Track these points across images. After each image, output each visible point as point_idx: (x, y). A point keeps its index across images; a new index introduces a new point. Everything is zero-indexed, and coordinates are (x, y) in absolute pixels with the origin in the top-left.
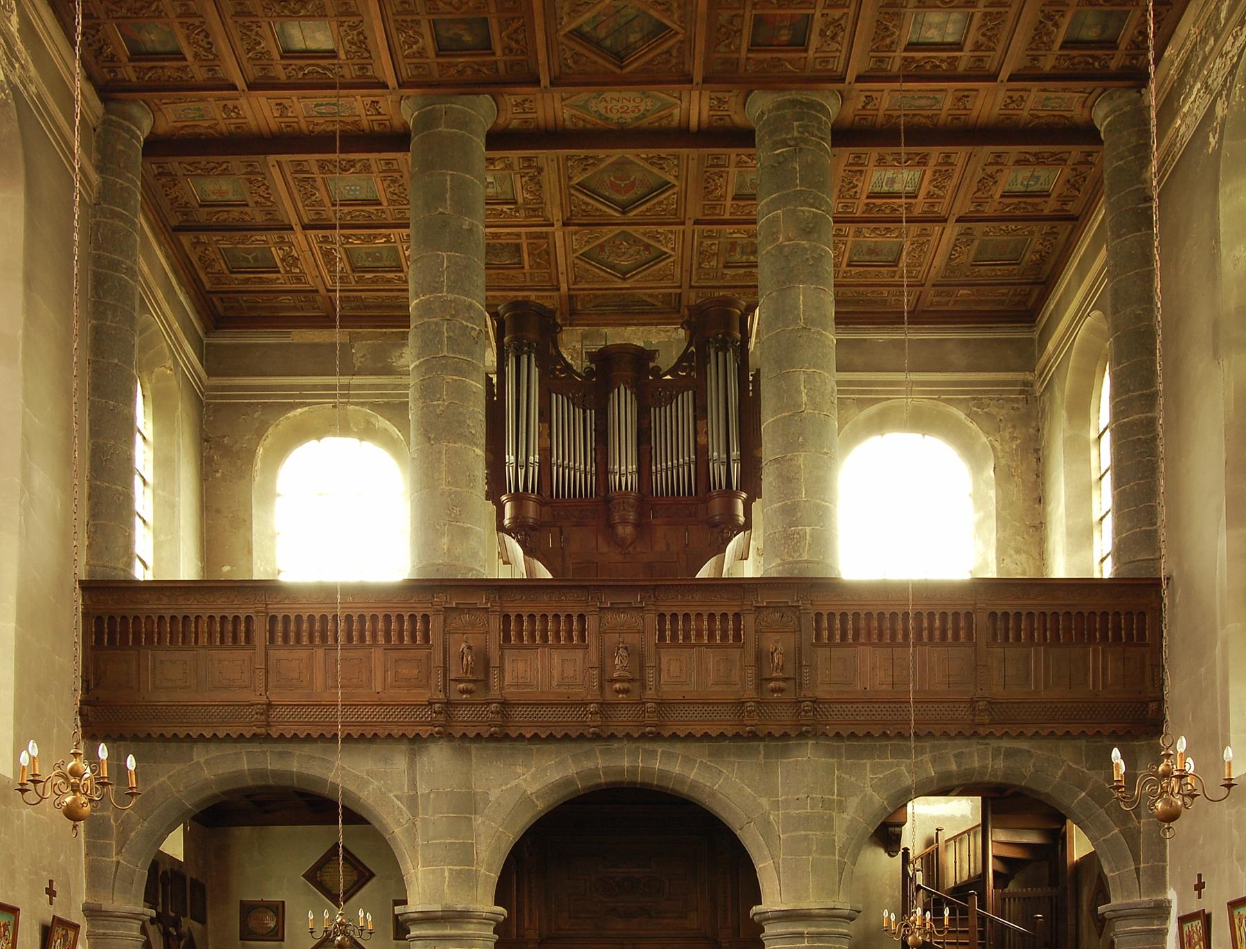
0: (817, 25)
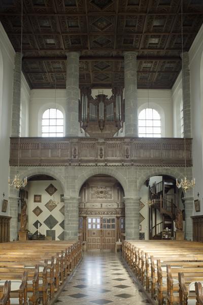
0: (134, 40)
